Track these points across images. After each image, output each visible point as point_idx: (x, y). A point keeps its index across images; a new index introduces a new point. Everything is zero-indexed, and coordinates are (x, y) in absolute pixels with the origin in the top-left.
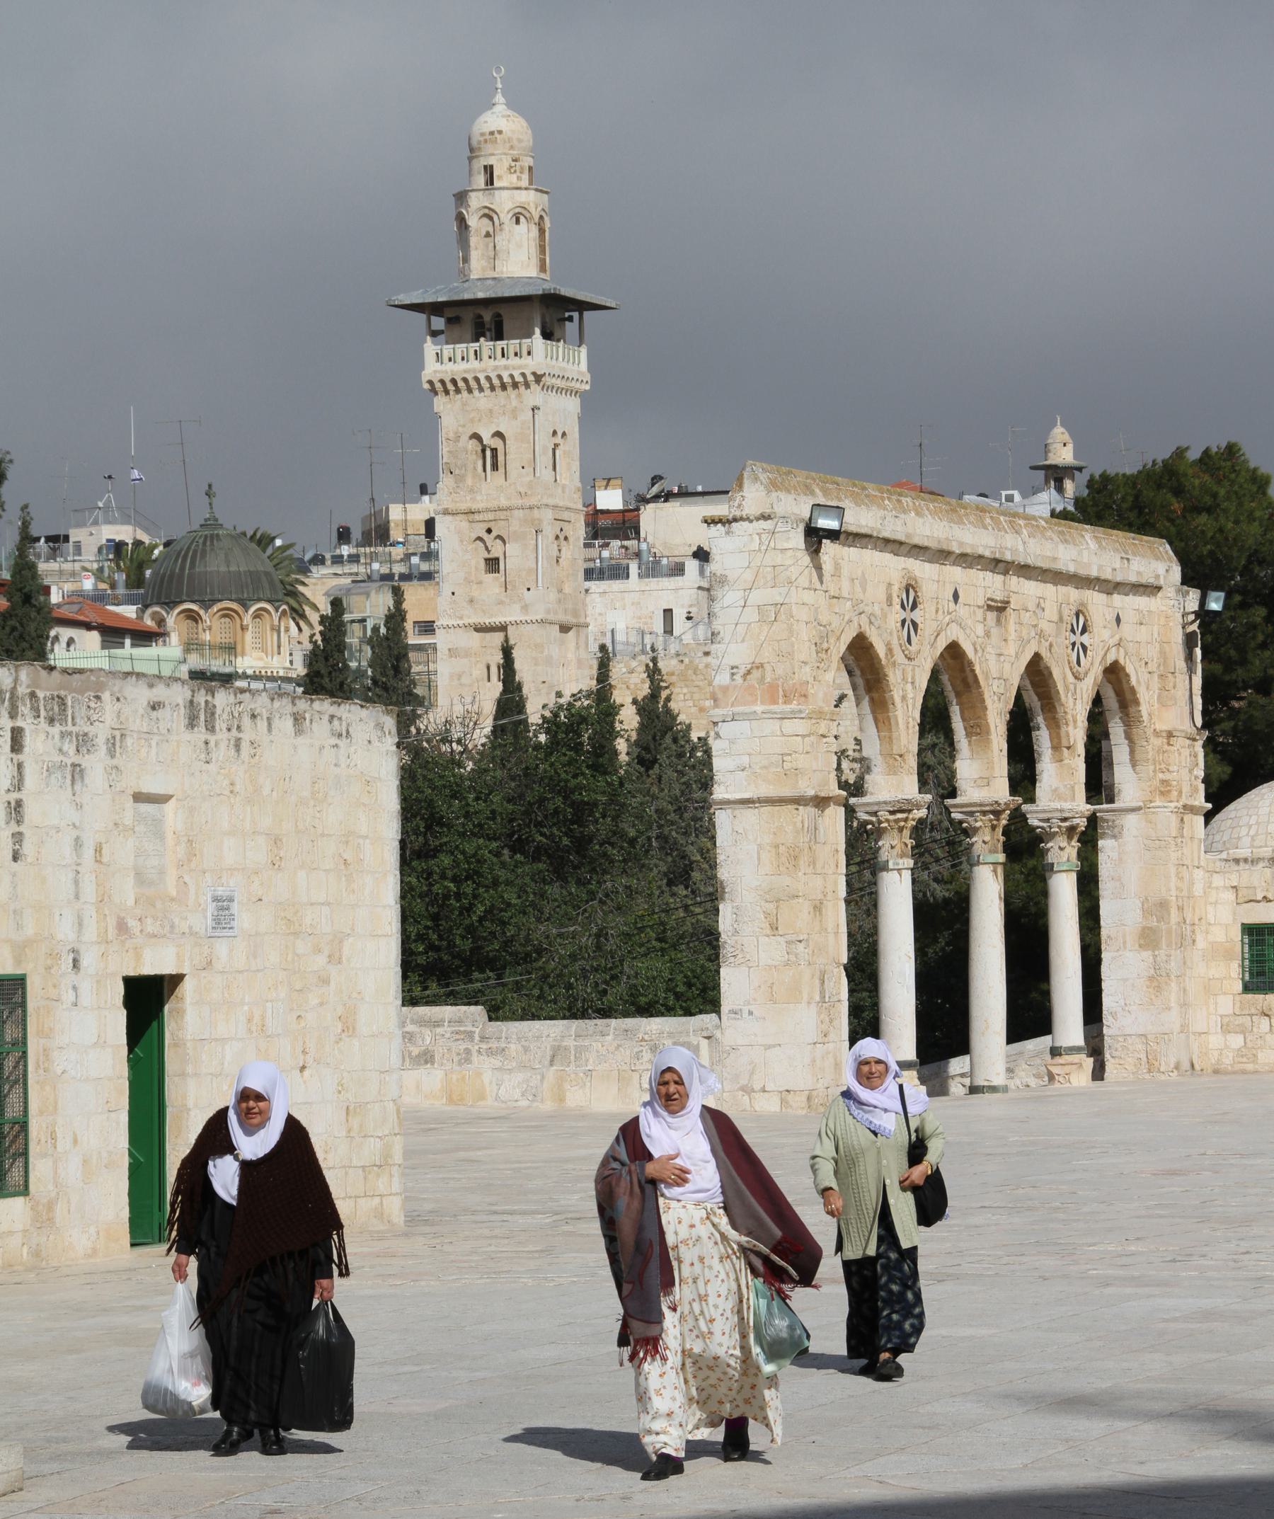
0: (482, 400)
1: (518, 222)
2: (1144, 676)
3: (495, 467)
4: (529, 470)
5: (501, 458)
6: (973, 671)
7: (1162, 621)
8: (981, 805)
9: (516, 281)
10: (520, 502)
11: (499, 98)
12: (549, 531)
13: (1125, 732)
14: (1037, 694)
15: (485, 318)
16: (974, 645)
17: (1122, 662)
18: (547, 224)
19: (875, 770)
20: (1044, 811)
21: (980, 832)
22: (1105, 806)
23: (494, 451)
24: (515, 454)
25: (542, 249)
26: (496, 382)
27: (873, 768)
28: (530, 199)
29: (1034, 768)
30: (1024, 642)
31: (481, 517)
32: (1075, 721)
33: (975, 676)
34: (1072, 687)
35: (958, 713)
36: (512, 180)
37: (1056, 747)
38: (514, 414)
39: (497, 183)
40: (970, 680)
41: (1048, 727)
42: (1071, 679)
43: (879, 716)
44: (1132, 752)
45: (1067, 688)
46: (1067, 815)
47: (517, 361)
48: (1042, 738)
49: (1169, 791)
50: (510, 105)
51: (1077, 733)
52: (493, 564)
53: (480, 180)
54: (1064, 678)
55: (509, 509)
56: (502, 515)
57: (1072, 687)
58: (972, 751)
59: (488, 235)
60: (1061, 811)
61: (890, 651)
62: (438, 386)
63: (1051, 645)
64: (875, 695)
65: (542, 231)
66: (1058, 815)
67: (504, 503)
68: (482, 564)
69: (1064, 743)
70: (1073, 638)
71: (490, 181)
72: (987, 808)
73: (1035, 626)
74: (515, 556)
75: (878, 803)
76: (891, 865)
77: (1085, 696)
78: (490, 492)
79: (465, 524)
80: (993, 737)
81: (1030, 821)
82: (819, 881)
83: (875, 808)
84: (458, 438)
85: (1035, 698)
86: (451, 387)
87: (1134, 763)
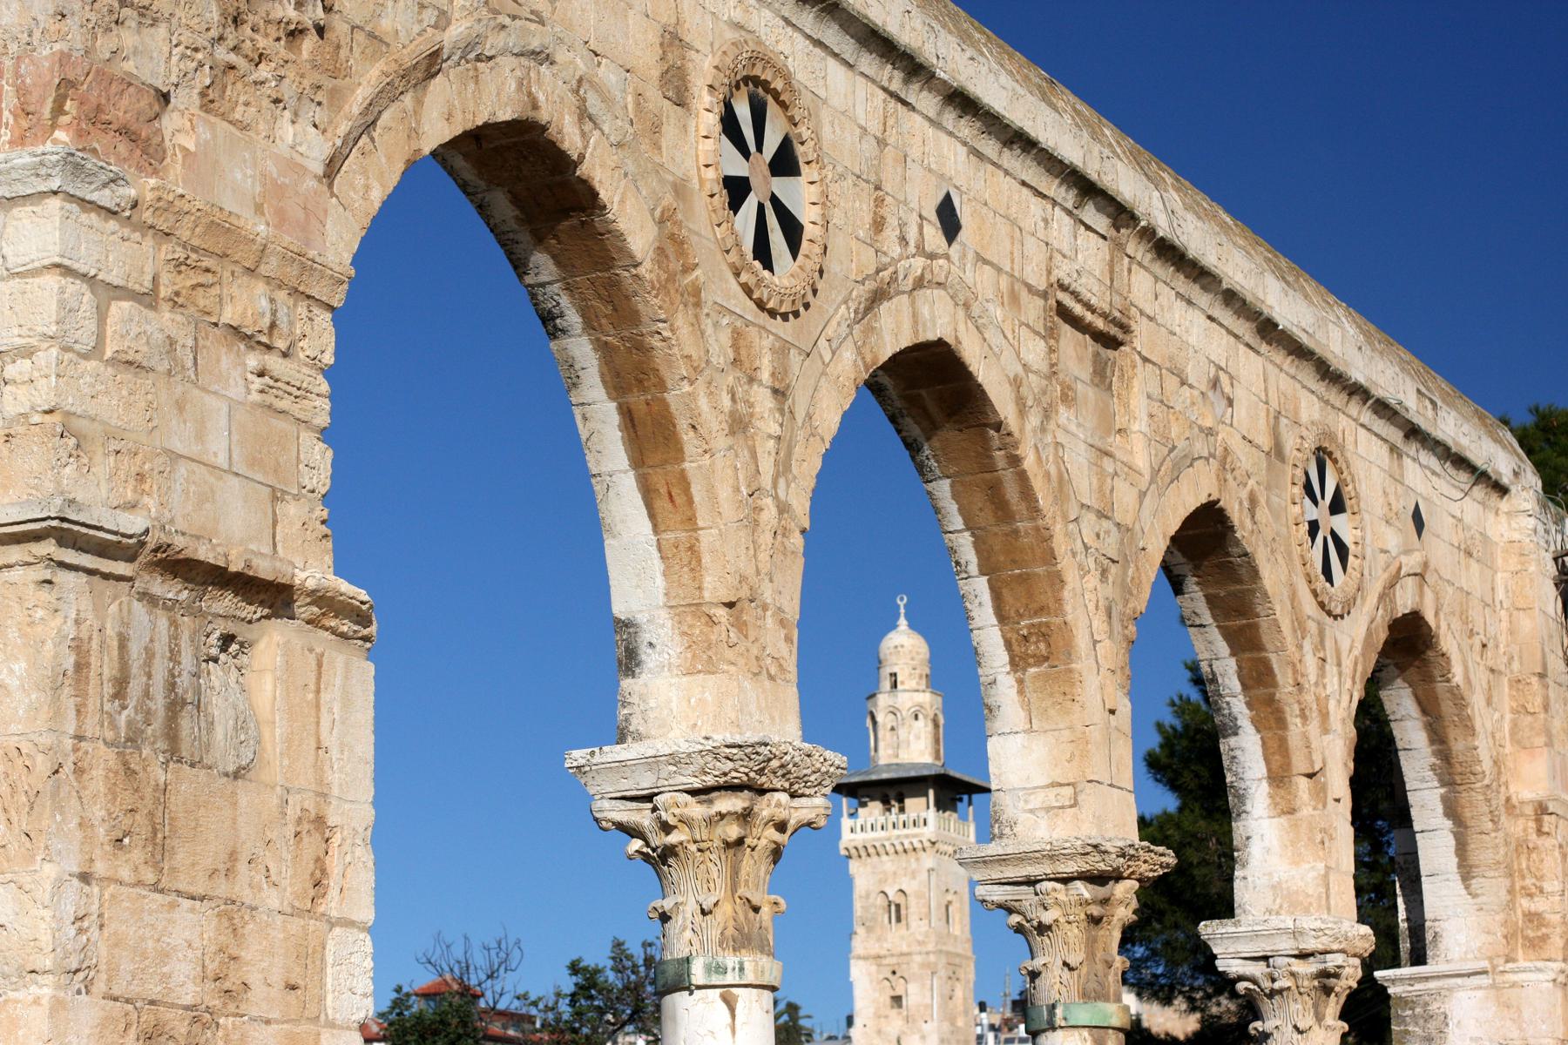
0: (888, 864)
1: (916, 717)
2: (1480, 677)
3: (899, 920)
4: (925, 922)
5: (903, 912)
6: (1015, 461)
7: (1514, 563)
8: (1052, 857)
9: (914, 766)
10: (919, 948)
11: (903, 623)
12: (943, 973)
13: (1445, 800)
14: (1228, 635)
15: (893, 790)
16: (1016, 383)
17: (1429, 617)
18: (941, 721)
19: (649, 659)
20: (1256, 935)
21: (1057, 935)
22: (1407, 971)
23: (898, 906)
24: (913, 910)
25: (937, 741)
26: (899, 848)
27: (646, 655)
28: (926, 698)
29: (1229, 833)
30: (1175, 465)
31: (887, 961)
32: (1324, 715)
33: (1023, 477)
34: (1312, 627)
35: (986, 597)
36: (913, 684)
37: (1279, 777)
38: (914, 875)
39: (899, 687)
40: (1012, 492)
41: (1258, 725)
42: (1309, 606)
43: (658, 480)
44: (1462, 849)
45: (1299, 625)
46: (1310, 944)
47: (916, 830)
48: (1246, 755)
49: (1544, 938)
50: (911, 626)
51: (1333, 750)
52: (897, 1000)
53: (886, 684)
54: (1293, 596)
55: (909, 954)
56: (905, 959)
57: (1312, 627)
58: (1027, 707)
59: (893, 729)
60: (1296, 934)
61: (673, 244)
62: (853, 852)
63: (1253, 501)
64: (637, 400)
65: (936, 725)
66: (1287, 945)
67: (905, 949)
68: (888, 1001)
69: (1299, 764)
70: (1312, 513)
71: (895, 685)
72: (1071, 867)
73: (1210, 432)
74: (915, 995)
75: (652, 762)
76: (698, 975)
77: (1347, 663)
78: (895, 939)
79: (874, 968)
80: (1083, 664)
81: (1221, 965)
82: (188, 931)
83: (645, 783)
84: (868, 896)
85: (1223, 647)
86: (865, 852)
87: (1466, 871)
